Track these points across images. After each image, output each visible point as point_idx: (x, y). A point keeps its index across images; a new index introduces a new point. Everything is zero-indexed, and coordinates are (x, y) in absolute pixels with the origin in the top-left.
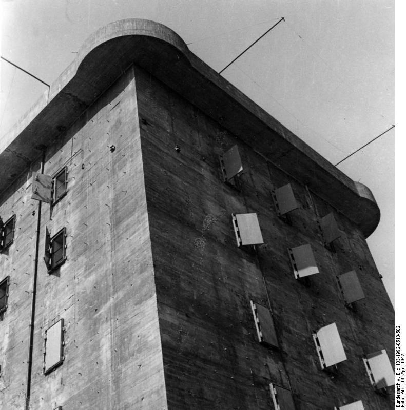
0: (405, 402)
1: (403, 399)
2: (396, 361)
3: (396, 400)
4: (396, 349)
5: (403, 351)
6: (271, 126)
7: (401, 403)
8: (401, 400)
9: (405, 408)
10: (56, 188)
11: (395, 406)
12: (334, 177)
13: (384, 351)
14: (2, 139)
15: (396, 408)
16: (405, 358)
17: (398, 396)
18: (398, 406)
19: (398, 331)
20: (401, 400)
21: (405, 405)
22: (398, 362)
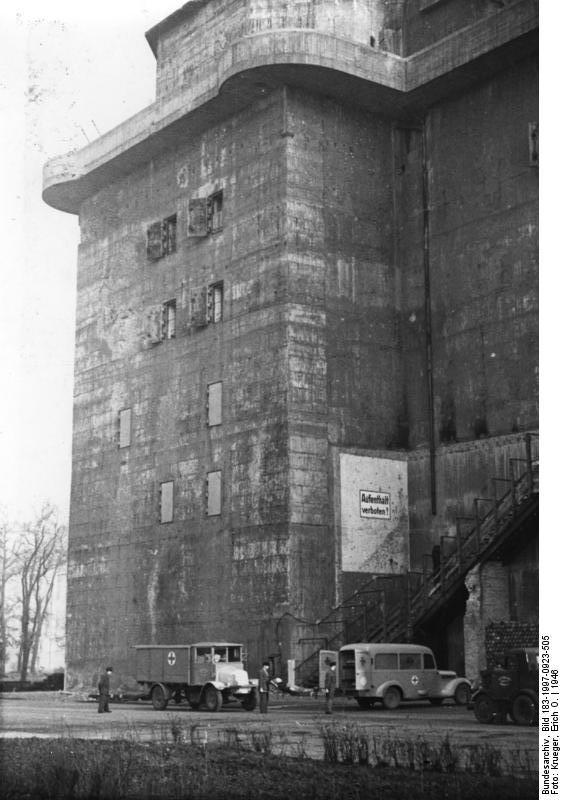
0: (559, 785)
1: (555, 779)
2: (541, 704)
3: (541, 780)
4: (540, 682)
5: (556, 663)
6: (361, 451)
7: (551, 786)
8: (551, 781)
9: (559, 797)
10: (25, 730)
11: (540, 792)
12: (433, 410)
13: (388, 69)
14: (238, 797)
15: (542, 797)
16: (559, 678)
17: (546, 772)
18: (545, 792)
19: (546, 646)
20: (551, 781)
21: (559, 791)
22: (545, 707)
